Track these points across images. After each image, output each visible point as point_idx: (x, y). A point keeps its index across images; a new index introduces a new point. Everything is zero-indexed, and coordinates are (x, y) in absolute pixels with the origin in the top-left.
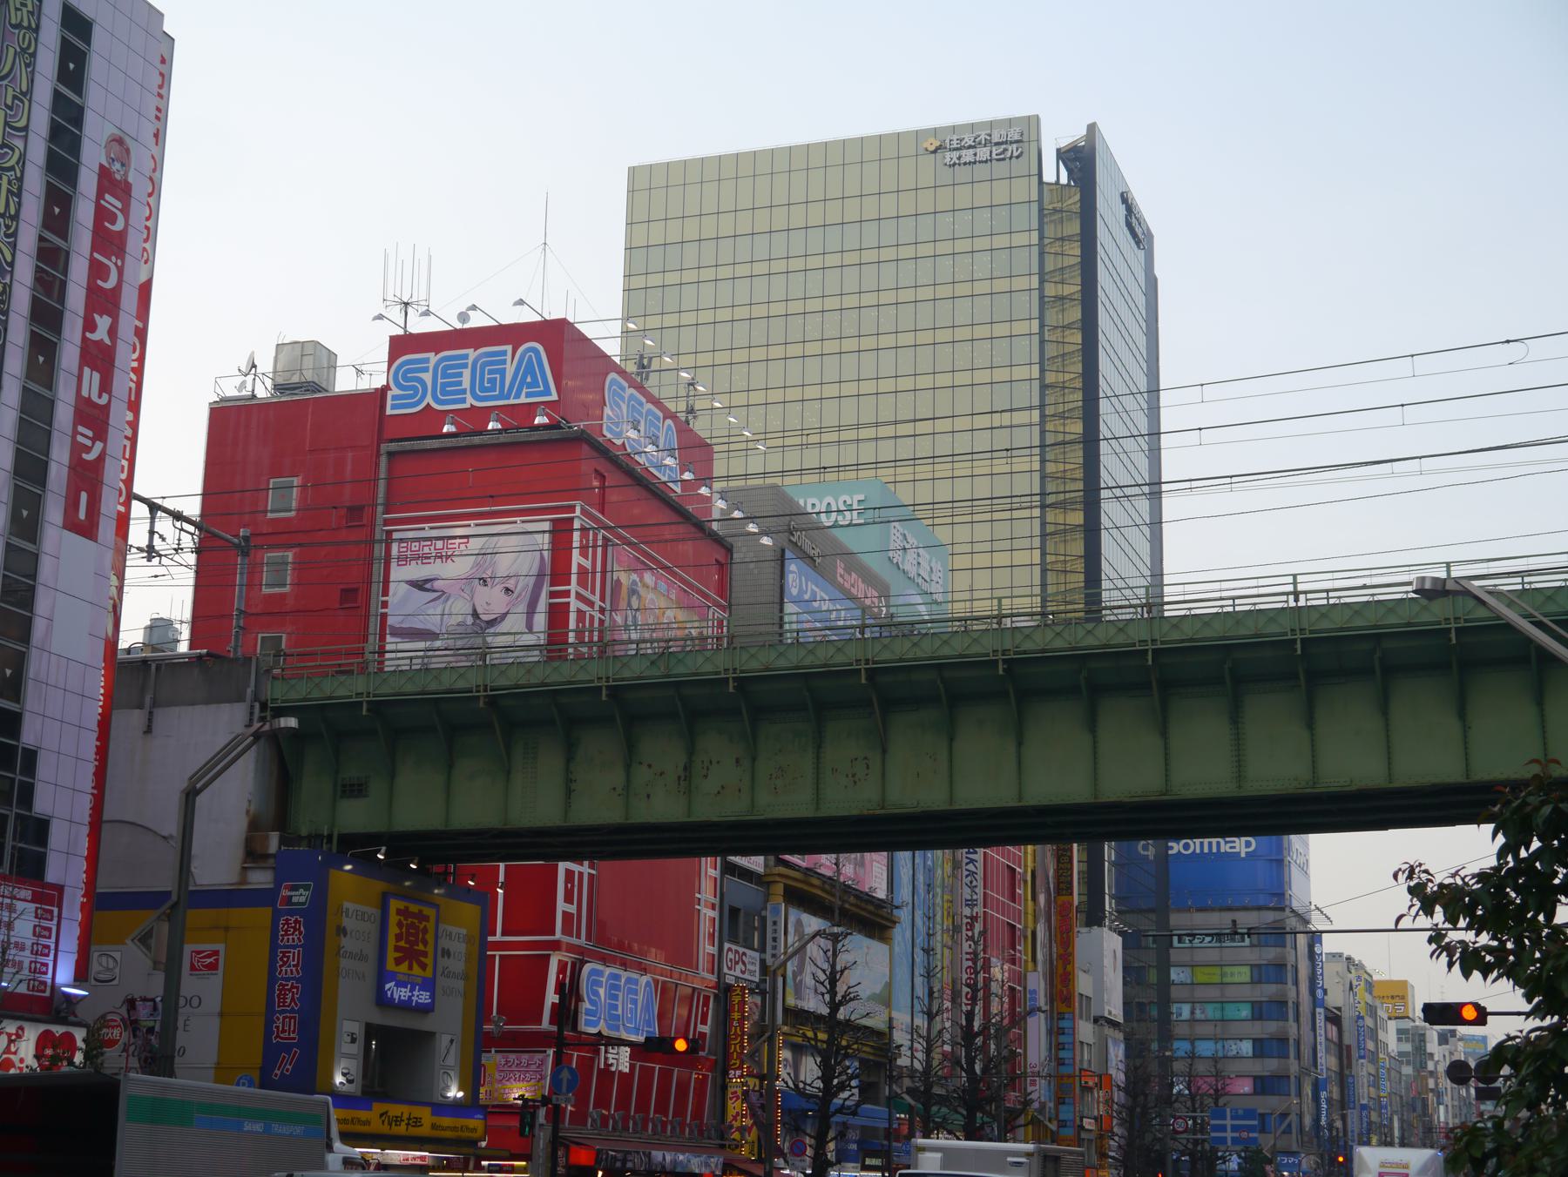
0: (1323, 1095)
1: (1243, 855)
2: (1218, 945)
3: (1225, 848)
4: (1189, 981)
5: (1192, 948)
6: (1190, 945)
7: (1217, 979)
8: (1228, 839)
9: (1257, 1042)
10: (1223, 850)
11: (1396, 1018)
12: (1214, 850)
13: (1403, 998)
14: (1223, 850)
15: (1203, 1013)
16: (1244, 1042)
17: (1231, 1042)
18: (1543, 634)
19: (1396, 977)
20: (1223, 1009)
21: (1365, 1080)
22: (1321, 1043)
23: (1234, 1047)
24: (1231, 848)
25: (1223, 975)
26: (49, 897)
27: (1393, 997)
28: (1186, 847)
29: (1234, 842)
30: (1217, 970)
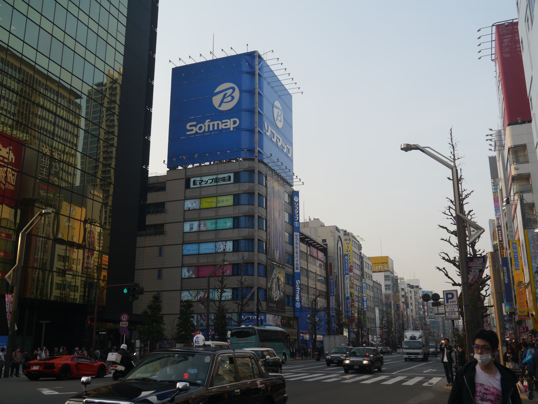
0: (297, 282)
1: (232, 129)
2: (215, 184)
3: (222, 126)
4: (198, 208)
5: (201, 187)
6: (199, 186)
7: (214, 205)
8: (223, 121)
9: (236, 243)
10: (220, 128)
11: (384, 271)
12: (216, 128)
13: (387, 263)
14: (220, 128)
15: (205, 226)
16: (228, 242)
17: (220, 243)
18: (442, 159)
19: (384, 255)
20: (216, 223)
21: (348, 285)
22: (297, 253)
23: (222, 246)
24: (225, 126)
25: (217, 202)
26: (505, 343)
27: (383, 263)
28: (200, 128)
29: (227, 122)
30: (214, 199)
